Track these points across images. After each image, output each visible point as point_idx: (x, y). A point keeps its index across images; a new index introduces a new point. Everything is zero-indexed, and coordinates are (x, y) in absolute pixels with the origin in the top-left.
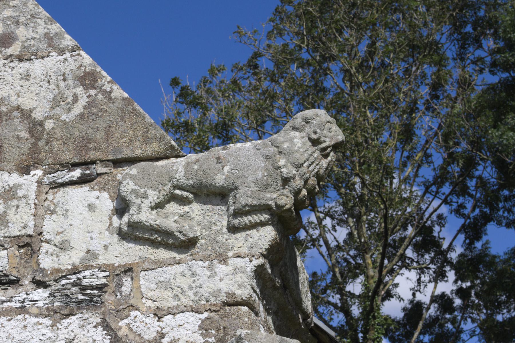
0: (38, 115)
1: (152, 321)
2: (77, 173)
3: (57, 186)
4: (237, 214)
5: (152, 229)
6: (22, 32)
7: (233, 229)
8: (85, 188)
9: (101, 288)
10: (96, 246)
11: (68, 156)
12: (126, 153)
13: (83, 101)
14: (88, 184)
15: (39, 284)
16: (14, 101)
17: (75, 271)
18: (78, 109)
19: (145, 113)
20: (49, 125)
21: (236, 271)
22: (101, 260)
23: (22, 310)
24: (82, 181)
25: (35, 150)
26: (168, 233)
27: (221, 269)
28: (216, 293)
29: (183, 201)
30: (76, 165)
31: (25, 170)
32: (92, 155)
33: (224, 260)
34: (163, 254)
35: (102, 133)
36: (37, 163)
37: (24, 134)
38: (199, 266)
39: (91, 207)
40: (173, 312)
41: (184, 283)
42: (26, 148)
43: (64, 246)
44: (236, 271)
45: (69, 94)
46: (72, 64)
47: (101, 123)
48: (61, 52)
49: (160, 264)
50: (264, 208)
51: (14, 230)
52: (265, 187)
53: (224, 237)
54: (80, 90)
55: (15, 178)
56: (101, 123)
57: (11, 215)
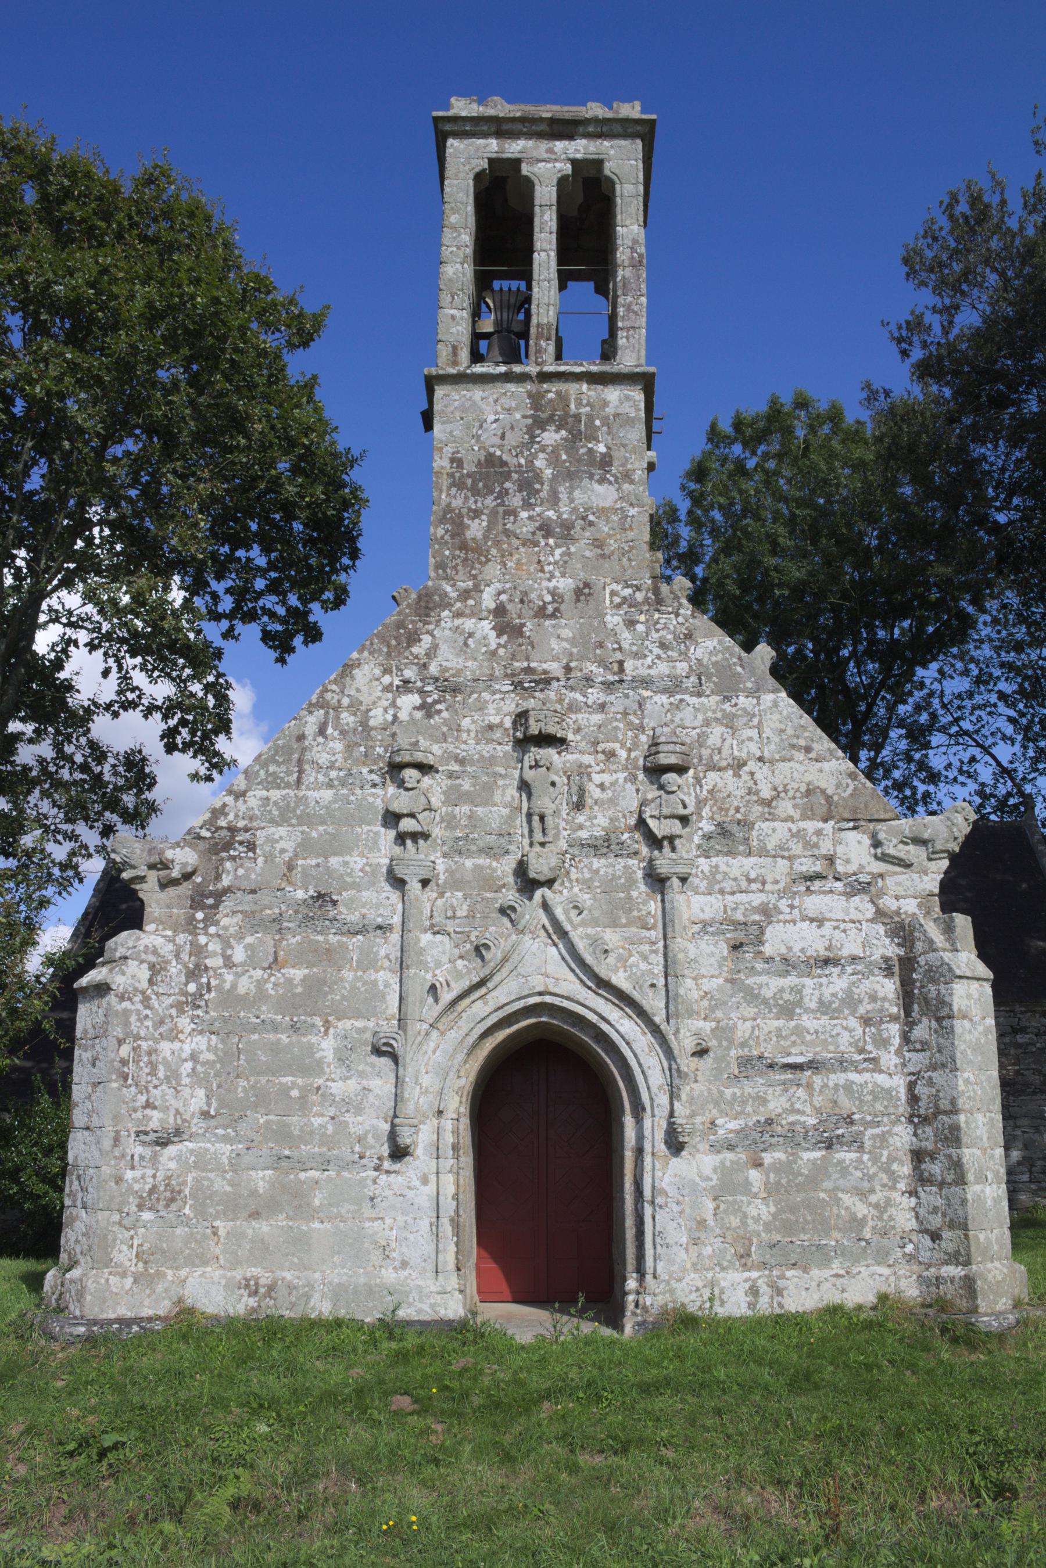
0: (829, 792)
1: (894, 901)
2: (851, 824)
3: (841, 830)
4: (933, 853)
5: (894, 857)
6: (815, 745)
7: (930, 859)
8: (855, 832)
9: (868, 883)
10: (864, 862)
11: (847, 815)
12: (876, 817)
13: (851, 787)
14: (621, 116)
15: (838, 879)
16: (816, 784)
17: (855, 874)
18: (849, 791)
19: (566, 108)
20: (836, 798)
21: (933, 880)
22: (867, 870)
23: (831, 892)
24: (855, 828)
25: (829, 811)
26: (902, 860)
27: (925, 878)
28: (924, 890)
29: (906, 844)
30: (849, 820)
31: (826, 821)
32: (859, 816)
33: (926, 874)
34: (897, 869)
35: (862, 806)
36: (832, 818)
37: (823, 802)
38: (915, 876)
39: (859, 842)
40: (904, 897)
41: (909, 884)
42: (825, 809)
43: (848, 861)
44: (933, 880)
45: (844, 782)
46: (843, 767)
47: (862, 800)
48: (838, 759)
49: (896, 873)
50: (948, 851)
51: (824, 851)
52: (947, 841)
53: (926, 863)
54: (849, 781)
55: (820, 825)
56: (862, 800)
57: (821, 843)
